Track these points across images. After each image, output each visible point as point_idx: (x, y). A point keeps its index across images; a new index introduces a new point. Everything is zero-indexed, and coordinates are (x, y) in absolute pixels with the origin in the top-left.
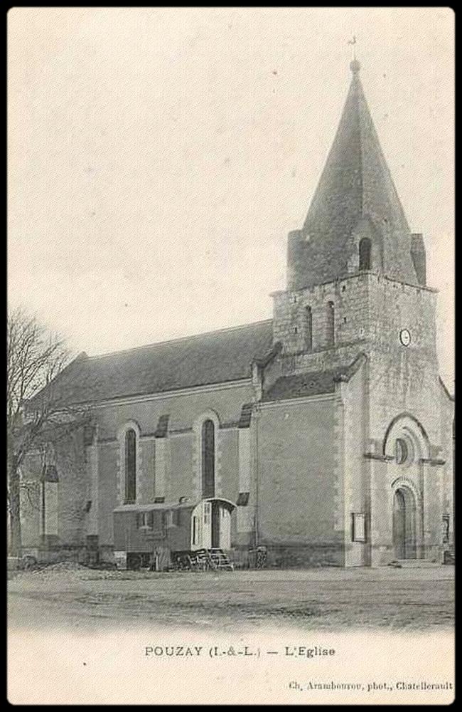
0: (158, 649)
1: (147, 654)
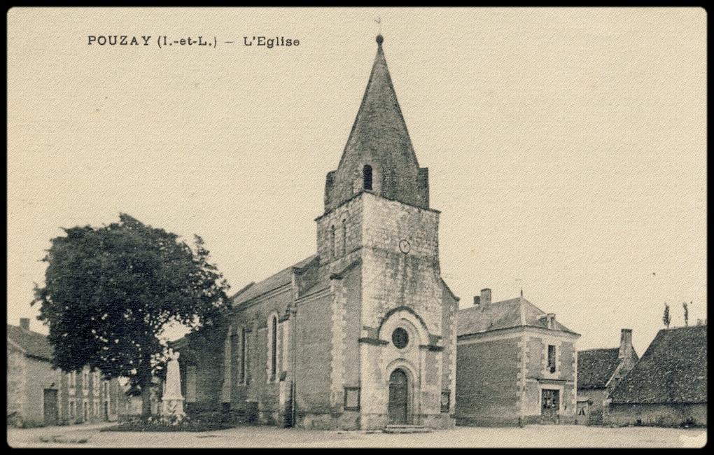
0: (101, 39)
1: (90, 44)
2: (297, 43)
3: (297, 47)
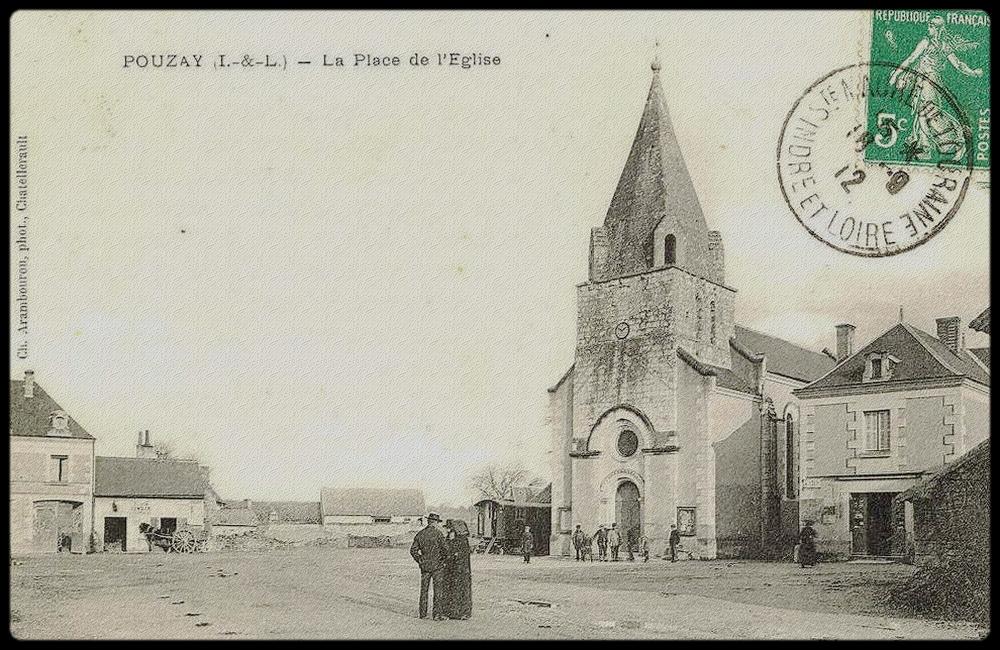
2: (497, 60)
3: (401, 61)
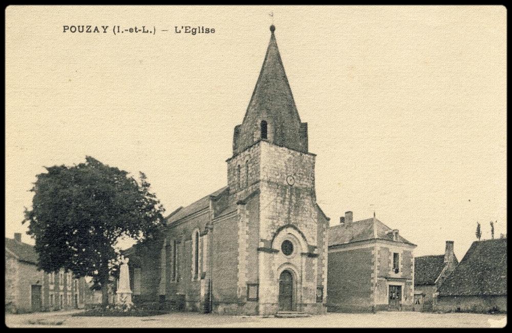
1: (64, 31)
